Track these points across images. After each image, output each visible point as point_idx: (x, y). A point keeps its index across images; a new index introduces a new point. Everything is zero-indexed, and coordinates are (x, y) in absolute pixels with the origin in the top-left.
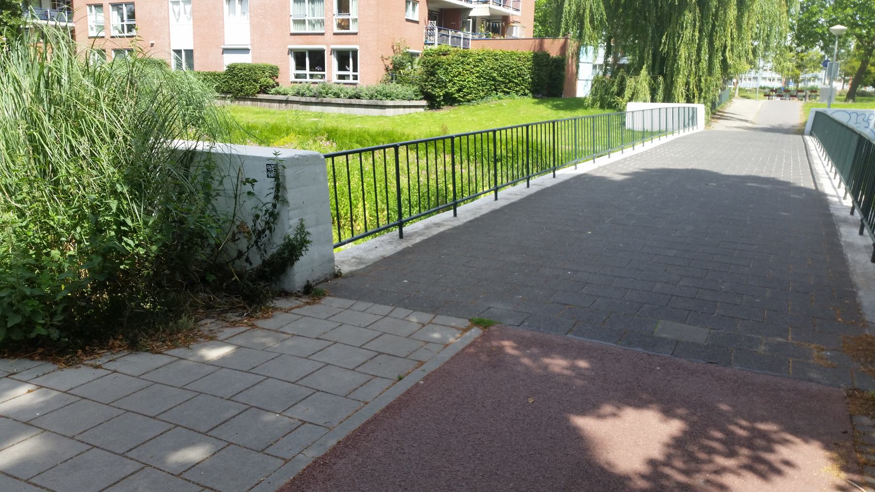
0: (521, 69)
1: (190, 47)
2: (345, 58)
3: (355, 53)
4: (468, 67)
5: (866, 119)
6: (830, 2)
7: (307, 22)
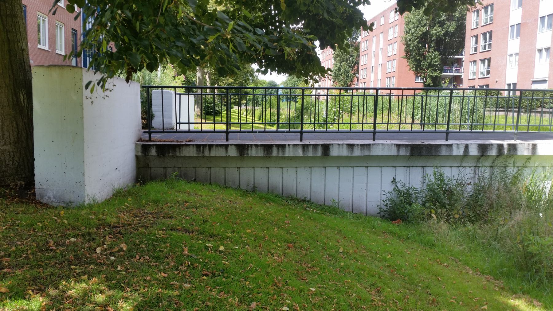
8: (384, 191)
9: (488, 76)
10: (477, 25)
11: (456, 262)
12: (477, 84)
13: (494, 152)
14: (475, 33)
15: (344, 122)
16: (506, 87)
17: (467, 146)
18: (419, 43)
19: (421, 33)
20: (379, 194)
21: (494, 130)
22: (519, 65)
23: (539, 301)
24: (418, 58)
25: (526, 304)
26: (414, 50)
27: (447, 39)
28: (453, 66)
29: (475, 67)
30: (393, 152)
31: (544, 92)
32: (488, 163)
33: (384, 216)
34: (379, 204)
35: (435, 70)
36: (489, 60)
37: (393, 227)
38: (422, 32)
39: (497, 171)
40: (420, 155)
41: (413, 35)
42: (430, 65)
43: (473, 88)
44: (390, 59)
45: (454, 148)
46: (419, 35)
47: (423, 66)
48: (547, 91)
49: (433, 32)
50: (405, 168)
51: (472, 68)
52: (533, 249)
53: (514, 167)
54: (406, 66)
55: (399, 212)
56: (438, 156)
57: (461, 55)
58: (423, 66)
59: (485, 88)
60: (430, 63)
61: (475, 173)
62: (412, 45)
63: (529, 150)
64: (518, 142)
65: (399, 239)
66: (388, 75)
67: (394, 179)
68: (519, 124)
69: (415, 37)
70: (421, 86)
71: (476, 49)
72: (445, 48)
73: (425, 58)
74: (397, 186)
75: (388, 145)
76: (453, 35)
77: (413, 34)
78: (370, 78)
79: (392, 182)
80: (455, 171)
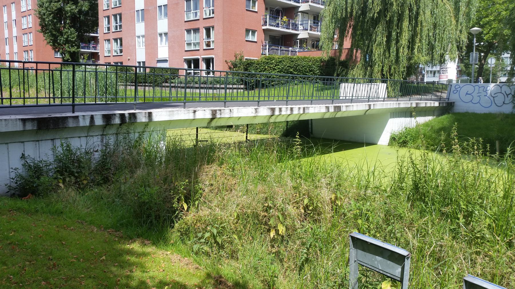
0: (312, 67)
1: (144, 60)
2: (209, 61)
3: (213, 59)
4: (272, 66)
5: (485, 90)
6: (106, 0)
7: (192, 44)
8: (12, 168)
9: (121, 54)
10: (108, 6)
11: (82, 224)
12: (112, 61)
13: (117, 121)
14: (107, 13)
15: (30, 97)
16: (137, 65)
17: (92, 117)
18: (54, 18)
19: (55, 8)
20: (8, 171)
21: (96, 102)
22: (145, 46)
23: (150, 240)
24: (54, 33)
25: (139, 245)
26: (50, 24)
27: (82, 17)
28: (90, 43)
29: (109, 45)
30: (19, 127)
31: (166, 69)
32: (113, 130)
33: (14, 194)
34: (8, 182)
35: (72, 46)
36: (121, 39)
37: (20, 203)
38: (56, 7)
39: (121, 137)
40: (48, 129)
41: (47, 10)
42: (67, 41)
43: (109, 64)
44: (25, 31)
45: (81, 119)
46: (53, 10)
47: (60, 41)
48: (168, 69)
49: (68, 8)
50: (34, 143)
51: (106, 46)
52: (145, 198)
53: (134, 133)
54: (43, 40)
55: (28, 187)
56: (66, 128)
57: (97, 33)
58: (60, 41)
59: (119, 64)
60: (67, 39)
61: (102, 141)
62: (47, 20)
63: (146, 118)
64: (137, 111)
65: (27, 214)
66: (26, 48)
67: (23, 155)
68: (137, 96)
69: (49, 11)
70: (60, 61)
71: (109, 29)
72: (80, 26)
73: (61, 34)
74: (26, 161)
75: (12, 120)
76: (86, 14)
77: (46, 8)
78: (4, 50)
79: (21, 158)
80: (83, 140)
